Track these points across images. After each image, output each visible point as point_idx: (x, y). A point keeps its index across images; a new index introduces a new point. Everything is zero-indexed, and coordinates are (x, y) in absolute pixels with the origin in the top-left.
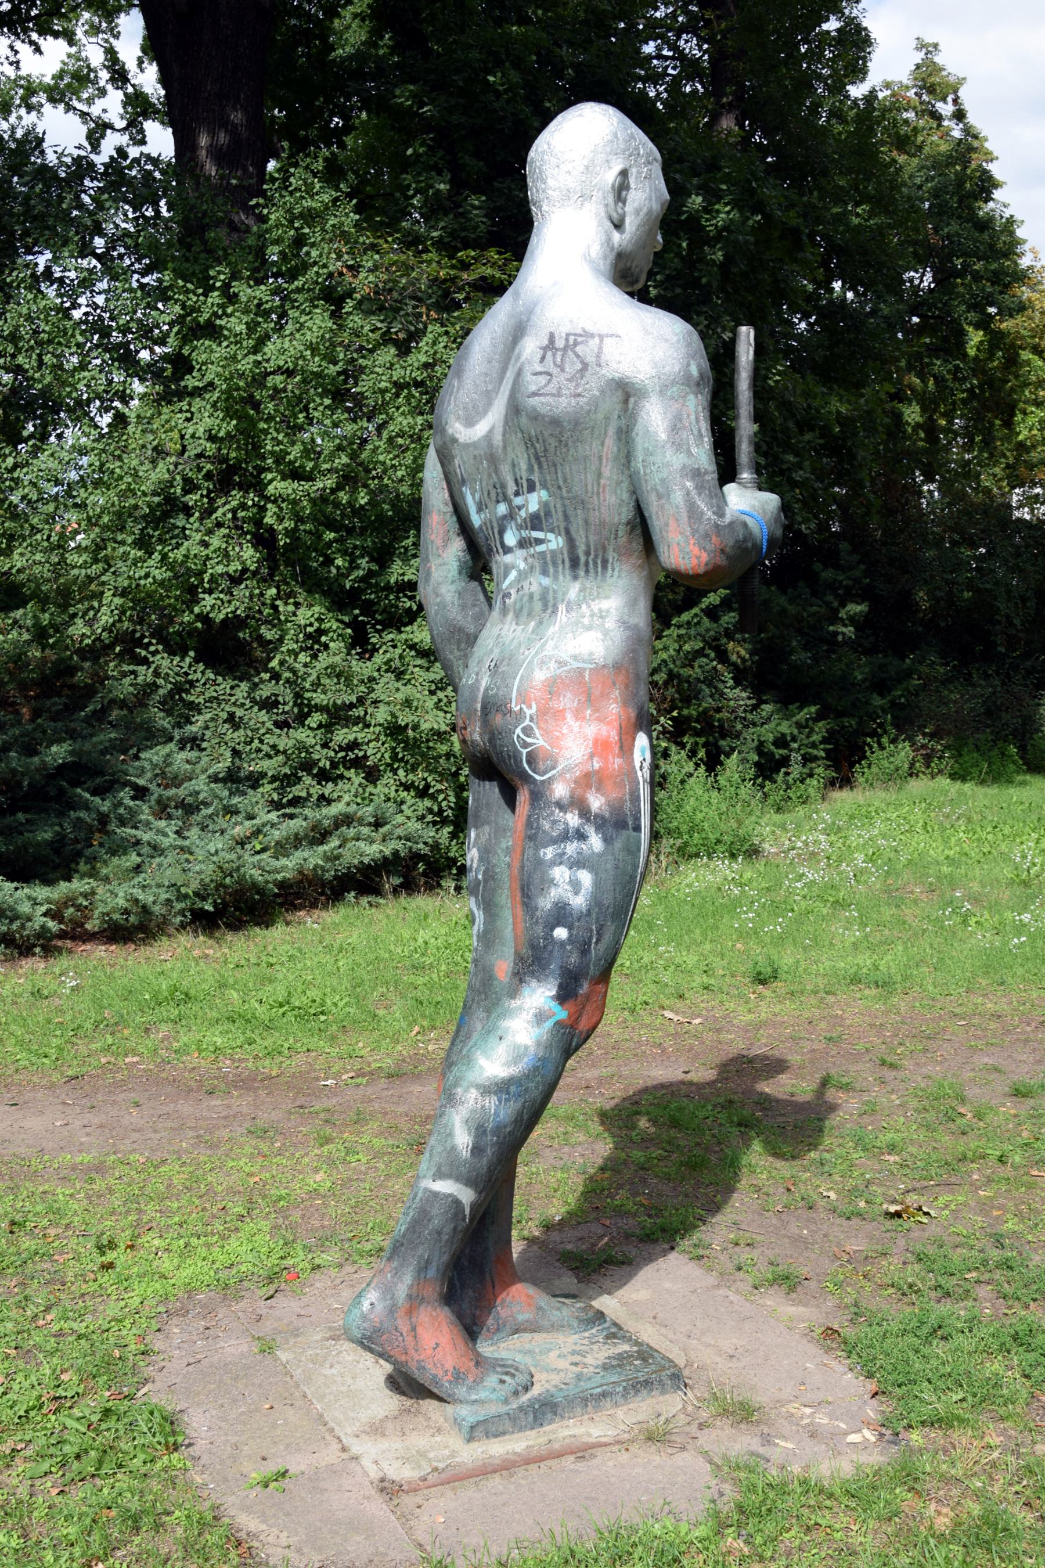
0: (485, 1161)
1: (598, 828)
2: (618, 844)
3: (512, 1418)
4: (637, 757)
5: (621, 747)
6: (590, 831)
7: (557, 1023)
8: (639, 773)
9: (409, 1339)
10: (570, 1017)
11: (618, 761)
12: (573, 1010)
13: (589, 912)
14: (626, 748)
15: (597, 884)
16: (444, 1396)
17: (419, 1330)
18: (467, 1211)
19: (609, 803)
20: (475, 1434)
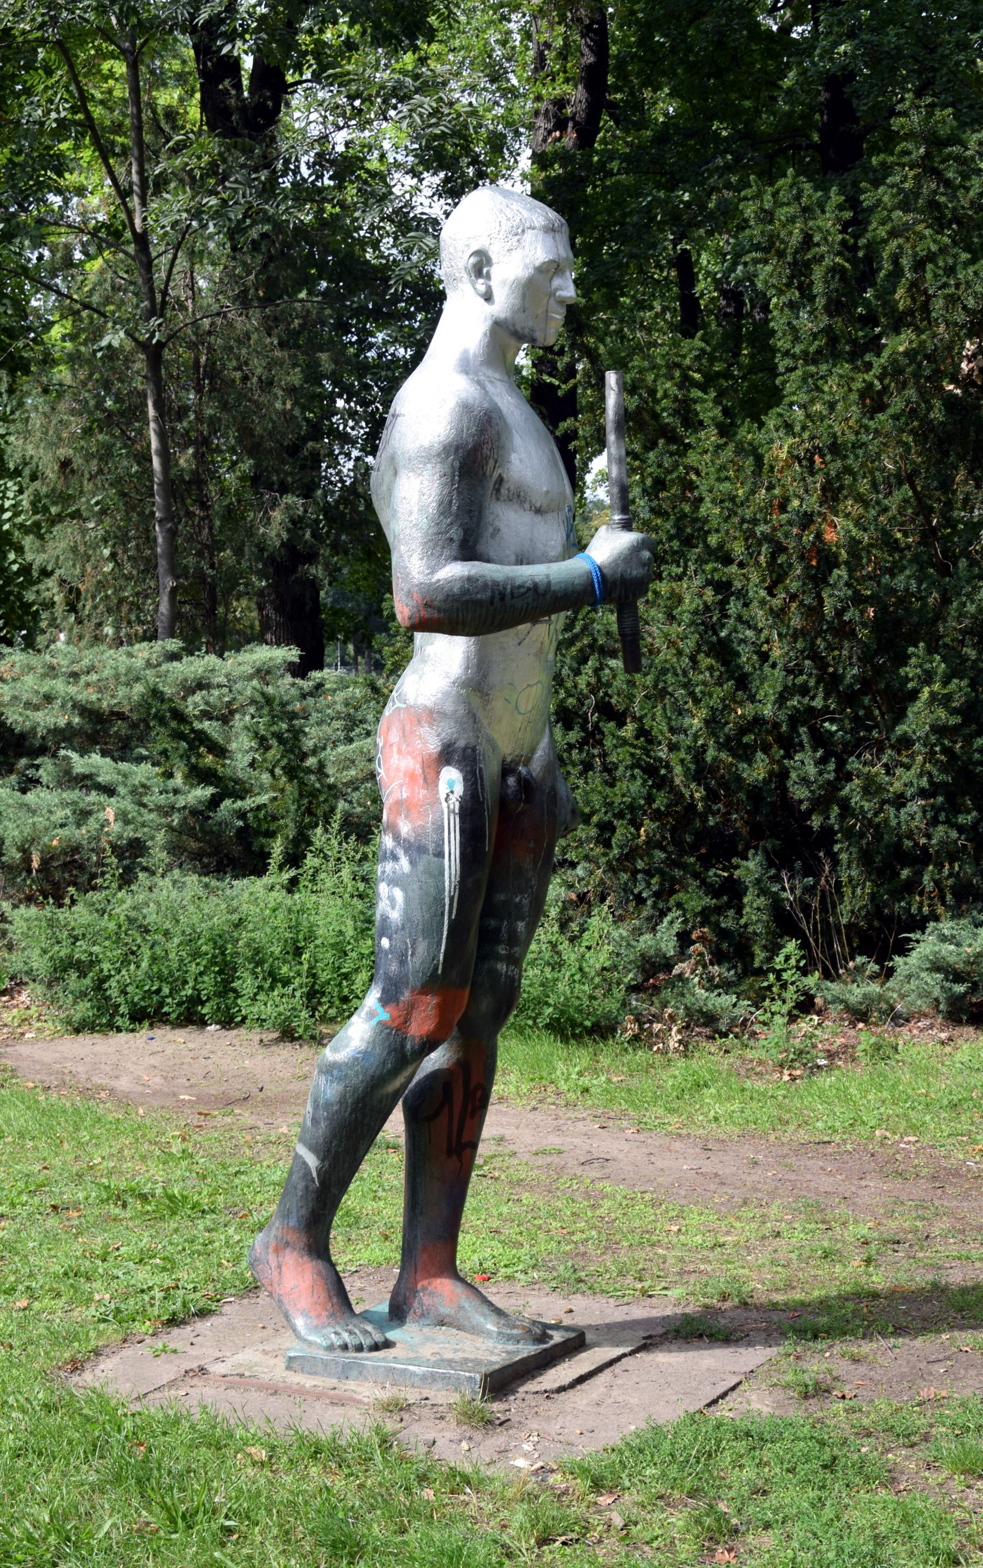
0: (320, 1132)
1: (407, 851)
2: (420, 868)
3: (325, 1364)
4: (443, 789)
5: (425, 779)
6: (400, 853)
7: (380, 1023)
8: (444, 805)
9: (275, 1274)
10: (393, 1019)
11: (423, 792)
12: (396, 1013)
13: (403, 928)
14: (431, 780)
15: (407, 901)
16: (198, 1300)
17: (284, 1269)
18: (315, 1174)
19: (413, 829)
20: (294, 1365)
